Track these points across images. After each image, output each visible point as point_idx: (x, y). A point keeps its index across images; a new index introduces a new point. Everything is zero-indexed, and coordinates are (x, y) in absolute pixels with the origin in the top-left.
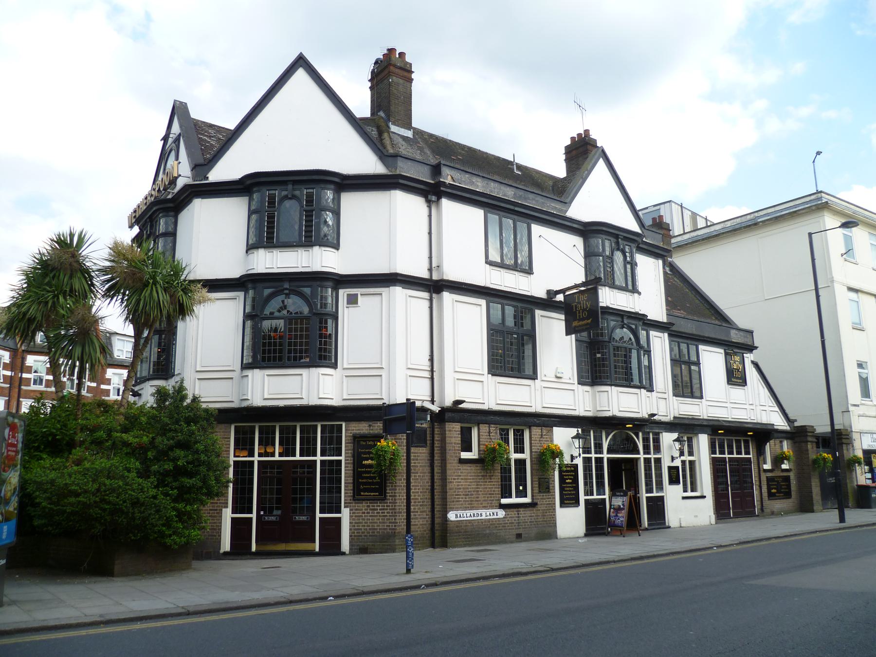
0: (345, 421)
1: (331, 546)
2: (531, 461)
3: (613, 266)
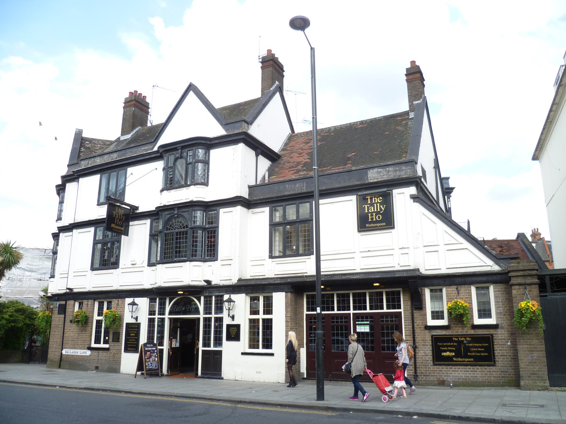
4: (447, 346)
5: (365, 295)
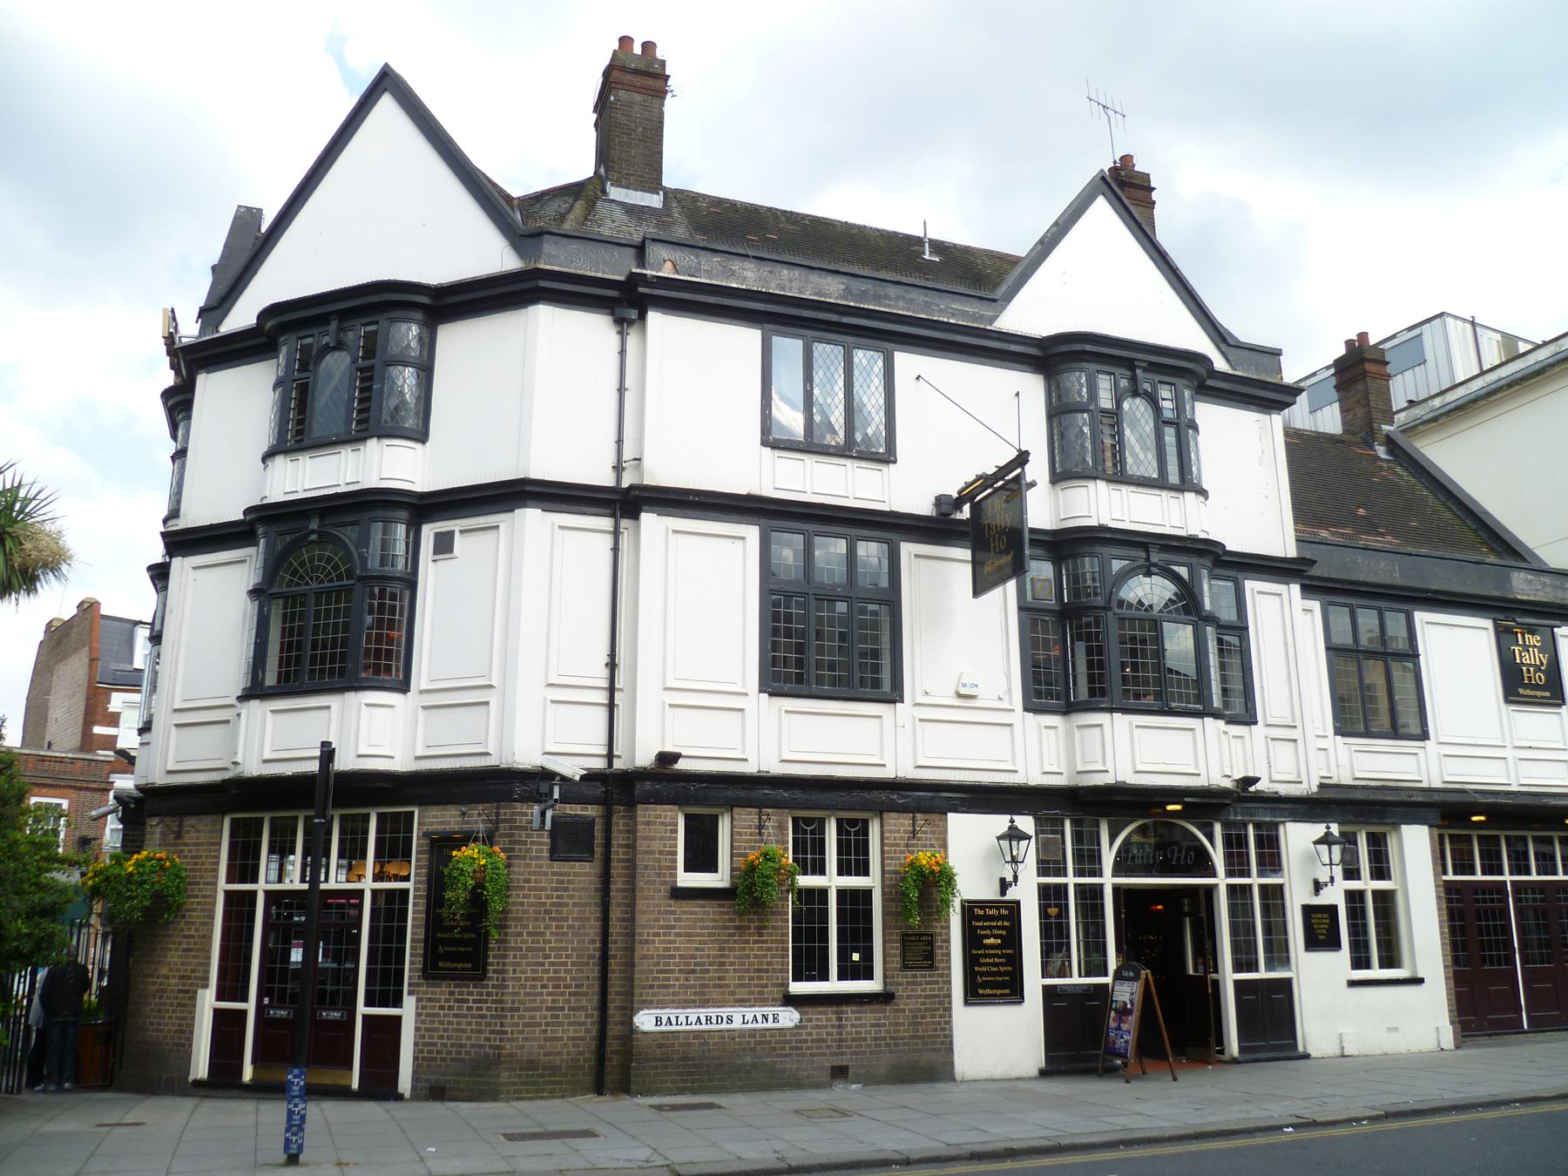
1: (380, 1085)
2: (884, 894)
3: (1120, 433)
4: (991, 928)
5: (366, 818)
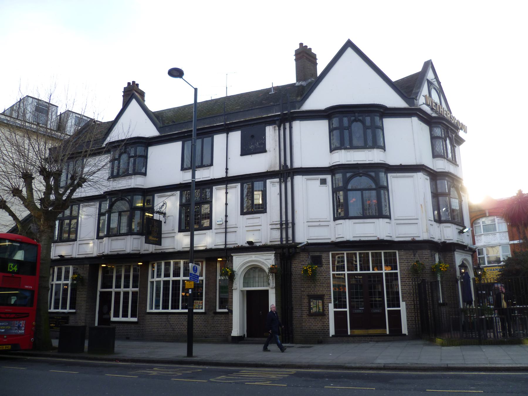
0: (398, 250)
